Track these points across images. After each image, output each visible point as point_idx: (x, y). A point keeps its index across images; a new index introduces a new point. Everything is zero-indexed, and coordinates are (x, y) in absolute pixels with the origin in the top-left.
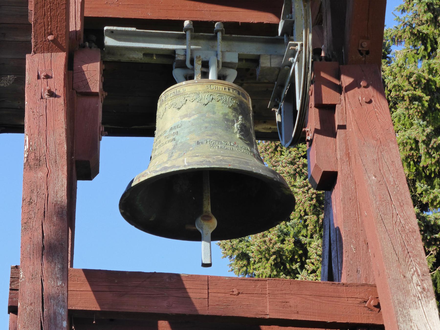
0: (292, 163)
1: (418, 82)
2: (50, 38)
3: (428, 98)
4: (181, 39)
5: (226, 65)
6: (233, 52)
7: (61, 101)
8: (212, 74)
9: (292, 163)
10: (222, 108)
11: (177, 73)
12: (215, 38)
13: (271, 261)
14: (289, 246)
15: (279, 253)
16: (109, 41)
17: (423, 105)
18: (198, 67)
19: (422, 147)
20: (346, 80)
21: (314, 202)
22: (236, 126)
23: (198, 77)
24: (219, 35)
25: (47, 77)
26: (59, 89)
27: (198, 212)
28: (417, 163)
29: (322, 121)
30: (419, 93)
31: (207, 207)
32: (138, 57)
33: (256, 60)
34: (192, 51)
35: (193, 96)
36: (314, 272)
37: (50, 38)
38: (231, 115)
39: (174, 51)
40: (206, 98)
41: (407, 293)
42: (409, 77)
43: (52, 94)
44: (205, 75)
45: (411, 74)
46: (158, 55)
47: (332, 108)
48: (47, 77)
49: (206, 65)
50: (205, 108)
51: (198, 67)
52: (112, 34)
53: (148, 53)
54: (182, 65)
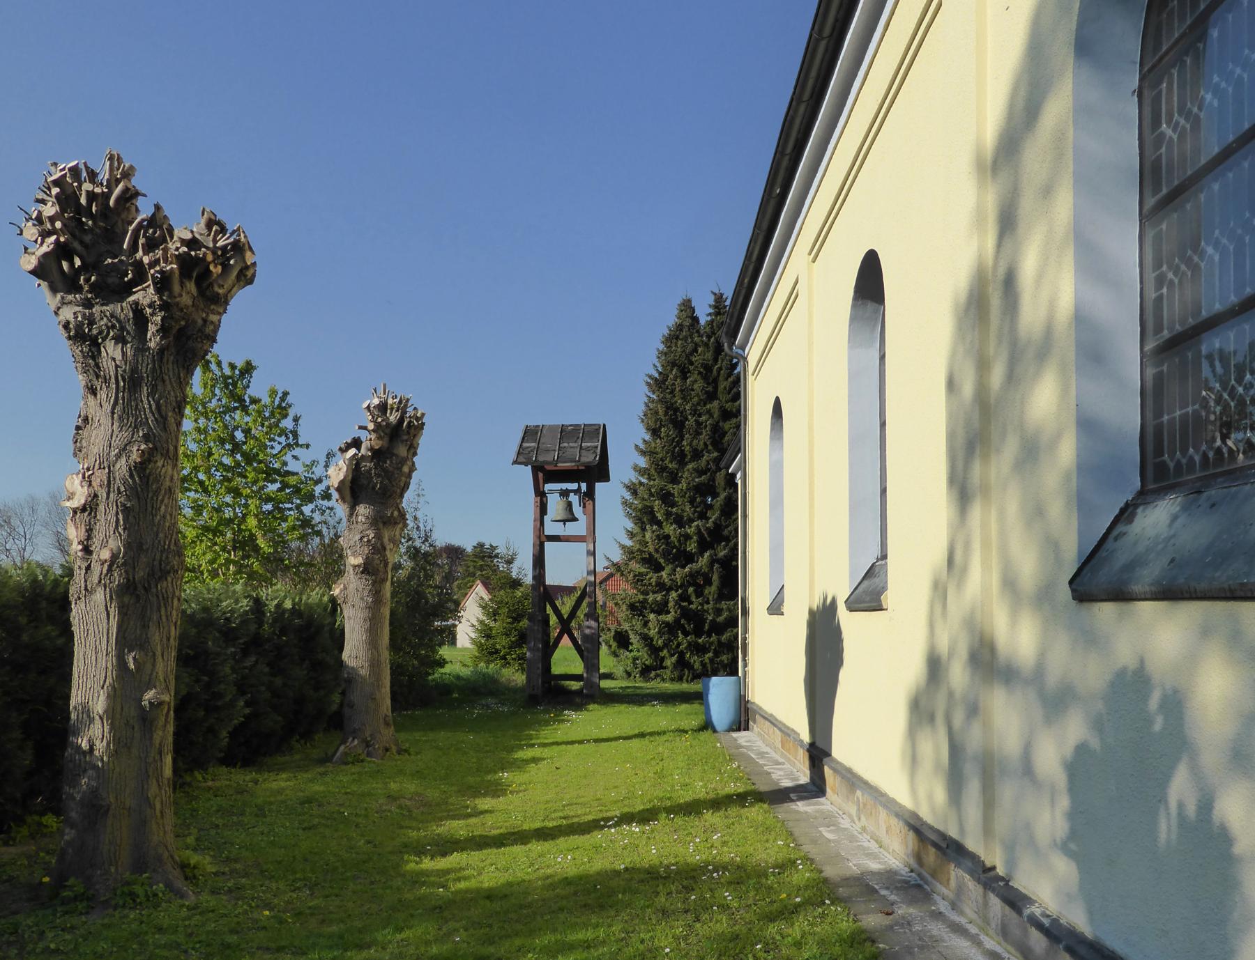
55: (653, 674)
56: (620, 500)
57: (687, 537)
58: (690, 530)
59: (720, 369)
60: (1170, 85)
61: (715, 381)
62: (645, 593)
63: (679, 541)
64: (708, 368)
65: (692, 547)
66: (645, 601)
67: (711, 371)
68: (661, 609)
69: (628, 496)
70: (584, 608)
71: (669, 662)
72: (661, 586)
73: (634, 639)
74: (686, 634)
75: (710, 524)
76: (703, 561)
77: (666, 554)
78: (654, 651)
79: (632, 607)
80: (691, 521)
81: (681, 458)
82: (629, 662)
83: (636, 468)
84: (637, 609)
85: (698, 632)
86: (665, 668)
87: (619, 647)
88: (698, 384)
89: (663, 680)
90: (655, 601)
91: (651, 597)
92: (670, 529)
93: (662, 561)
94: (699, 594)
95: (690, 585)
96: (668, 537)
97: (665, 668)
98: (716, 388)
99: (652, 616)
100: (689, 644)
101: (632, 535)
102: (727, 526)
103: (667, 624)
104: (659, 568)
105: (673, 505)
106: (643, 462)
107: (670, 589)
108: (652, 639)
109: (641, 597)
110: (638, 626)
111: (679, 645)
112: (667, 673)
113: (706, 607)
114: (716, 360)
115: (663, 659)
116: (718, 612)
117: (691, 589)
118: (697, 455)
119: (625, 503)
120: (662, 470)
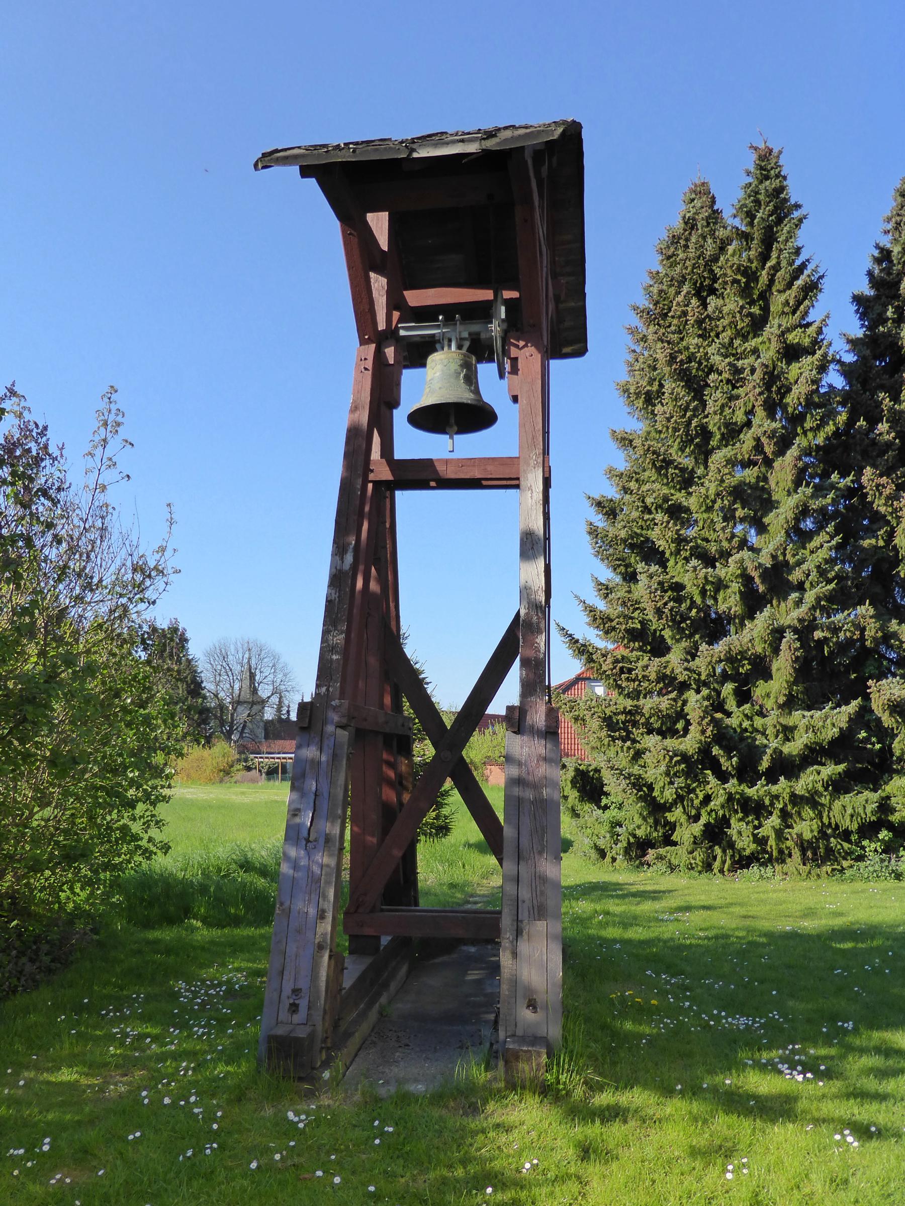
0: (656, 333)
1: (738, 269)
3: (744, 280)
4: (438, 327)
5: (462, 339)
6: (464, 331)
7: (370, 372)
9: (656, 333)
10: (455, 366)
11: (438, 346)
12: (456, 324)
15: (648, 393)
16: (402, 333)
17: (741, 286)
19: (738, 315)
20: (522, 343)
22: (462, 375)
23: (446, 348)
25: (365, 359)
26: (370, 367)
28: (736, 326)
30: (739, 277)
31: (452, 420)
32: (418, 339)
33: (478, 334)
34: (444, 333)
40: (446, 362)
41: (528, 465)
42: (731, 267)
43: (366, 369)
44: (450, 346)
45: (733, 264)
47: (516, 359)
48: (365, 359)
49: (450, 341)
51: (446, 342)
52: (403, 328)
54: (439, 341)
55: (651, 854)
56: (584, 528)
57: (720, 585)
58: (727, 571)
59: (776, 268)
60: (363, 1015)
61: (765, 296)
62: (635, 695)
63: (703, 592)
64: (751, 276)
65: (730, 602)
66: (637, 711)
67: (756, 280)
68: (671, 725)
69: (599, 521)
70: (509, 693)
71: (687, 833)
72: (669, 682)
73: (614, 786)
74: (723, 777)
75: (766, 560)
76: (752, 635)
77: (677, 621)
78: (656, 809)
79: (609, 723)
80: (725, 555)
81: (701, 444)
82: (604, 830)
83: (612, 473)
84: (620, 727)
85: (747, 772)
86: (675, 844)
87: (582, 799)
88: (728, 304)
89: (672, 868)
90: (657, 712)
91: (647, 704)
92: (688, 574)
93: (667, 634)
94: (743, 697)
95: (725, 677)
96: (678, 587)
97: (675, 844)
98: (766, 309)
99: (651, 741)
100: (730, 798)
101: (606, 590)
102: (799, 564)
103: (685, 758)
104: (659, 649)
105: (687, 523)
106: (621, 461)
107: (684, 687)
108: (651, 788)
109: (629, 703)
110: (623, 761)
111: (707, 799)
112: (679, 854)
113: (758, 722)
114: (764, 257)
115: (673, 827)
116: (787, 732)
117: (728, 688)
118: (732, 433)
119: (593, 532)
120: (663, 465)
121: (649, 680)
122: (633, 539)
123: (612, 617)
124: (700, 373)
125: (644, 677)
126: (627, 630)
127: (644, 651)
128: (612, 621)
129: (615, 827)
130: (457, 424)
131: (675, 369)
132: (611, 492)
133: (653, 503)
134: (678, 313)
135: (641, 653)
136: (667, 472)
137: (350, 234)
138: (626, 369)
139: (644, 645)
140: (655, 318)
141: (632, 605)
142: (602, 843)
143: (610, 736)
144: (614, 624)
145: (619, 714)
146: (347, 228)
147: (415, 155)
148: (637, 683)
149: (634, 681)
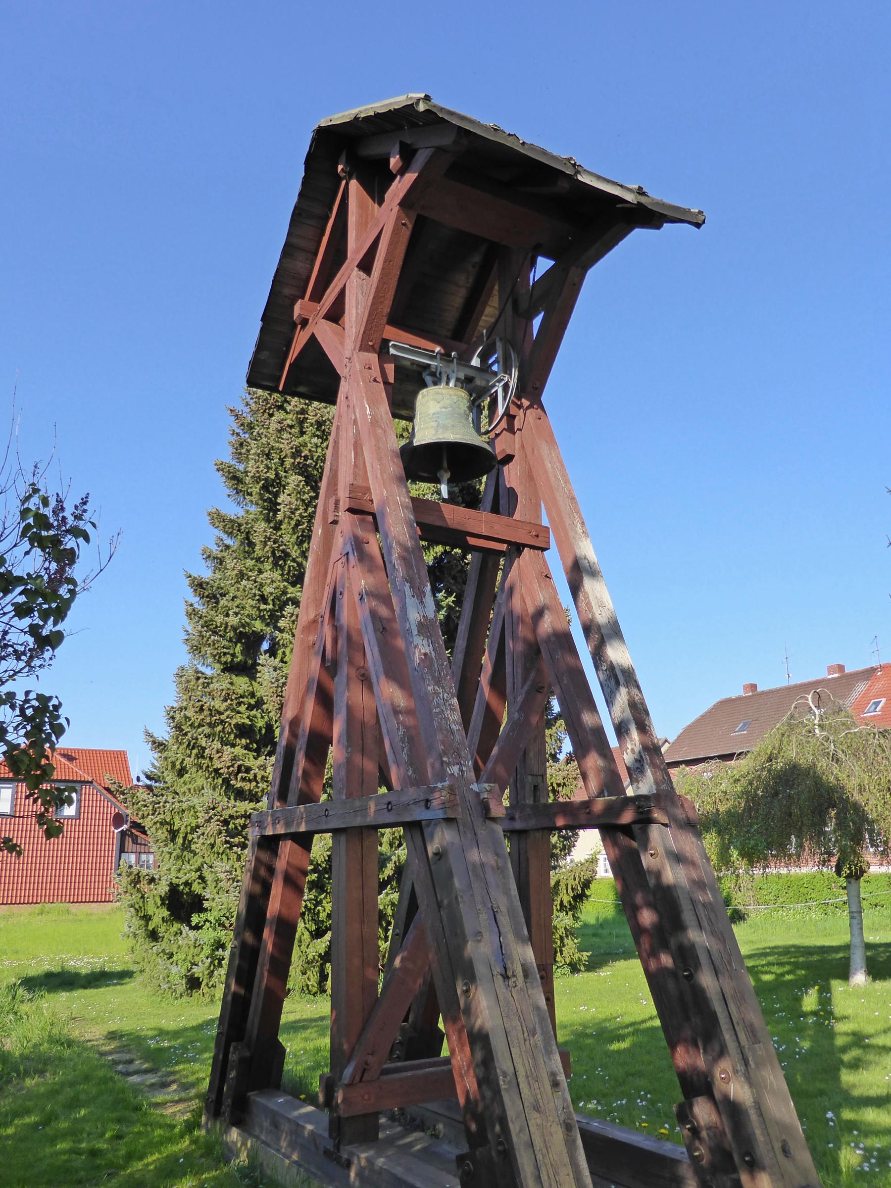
2: (371, 343)
8: (452, 384)
12: (452, 361)
13: (261, 484)
14: (272, 475)
18: (444, 378)
21: (294, 450)
24: (455, 360)
27: (440, 467)
29: (508, 425)
31: (445, 465)
32: (408, 363)
35: (448, 396)
36: (289, 495)
37: (371, 343)
38: (468, 411)
39: (429, 365)
44: (447, 383)
46: (418, 365)
50: (455, 406)
51: (444, 378)
53: (413, 362)
56: (183, 609)
121: (267, 781)
122: (244, 628)
123: (221, 709)
124: (315, 472)
125: (263, 777)
126: (237, 726)
127: (250, 750)
128: (221, 713)
129: (217, 949)
130: (450, 468)
131: (299, 463)
132: (206, 572)
133: (271, 594)
134: (298, 409)
135: (246, 752)
136: (285, 564)
137: (404, 224)
138: (231, 450)
139: (251, 743)
140: (270, 408)
141: (236, 698)
142: (197, 971)
143: (227, 842)
144: (223, 717)
145: (237, 818)
146: (403, 215)
147: (580, 178)
148: (254, 784)
149: (250, 781)
